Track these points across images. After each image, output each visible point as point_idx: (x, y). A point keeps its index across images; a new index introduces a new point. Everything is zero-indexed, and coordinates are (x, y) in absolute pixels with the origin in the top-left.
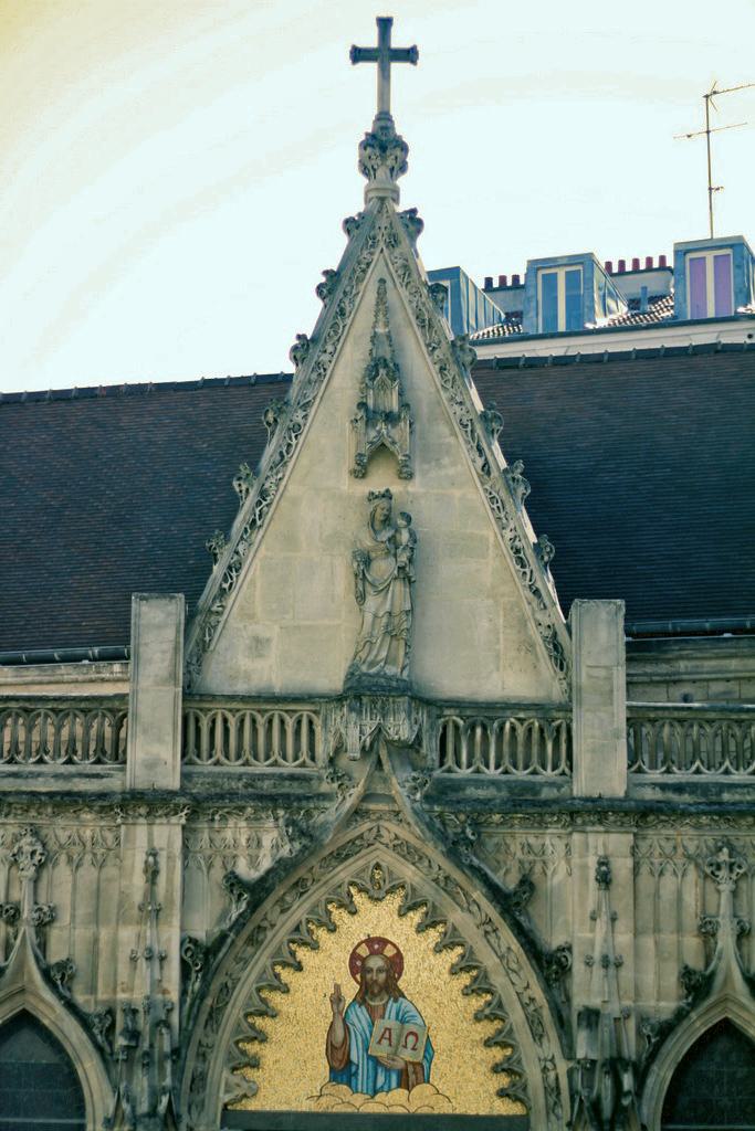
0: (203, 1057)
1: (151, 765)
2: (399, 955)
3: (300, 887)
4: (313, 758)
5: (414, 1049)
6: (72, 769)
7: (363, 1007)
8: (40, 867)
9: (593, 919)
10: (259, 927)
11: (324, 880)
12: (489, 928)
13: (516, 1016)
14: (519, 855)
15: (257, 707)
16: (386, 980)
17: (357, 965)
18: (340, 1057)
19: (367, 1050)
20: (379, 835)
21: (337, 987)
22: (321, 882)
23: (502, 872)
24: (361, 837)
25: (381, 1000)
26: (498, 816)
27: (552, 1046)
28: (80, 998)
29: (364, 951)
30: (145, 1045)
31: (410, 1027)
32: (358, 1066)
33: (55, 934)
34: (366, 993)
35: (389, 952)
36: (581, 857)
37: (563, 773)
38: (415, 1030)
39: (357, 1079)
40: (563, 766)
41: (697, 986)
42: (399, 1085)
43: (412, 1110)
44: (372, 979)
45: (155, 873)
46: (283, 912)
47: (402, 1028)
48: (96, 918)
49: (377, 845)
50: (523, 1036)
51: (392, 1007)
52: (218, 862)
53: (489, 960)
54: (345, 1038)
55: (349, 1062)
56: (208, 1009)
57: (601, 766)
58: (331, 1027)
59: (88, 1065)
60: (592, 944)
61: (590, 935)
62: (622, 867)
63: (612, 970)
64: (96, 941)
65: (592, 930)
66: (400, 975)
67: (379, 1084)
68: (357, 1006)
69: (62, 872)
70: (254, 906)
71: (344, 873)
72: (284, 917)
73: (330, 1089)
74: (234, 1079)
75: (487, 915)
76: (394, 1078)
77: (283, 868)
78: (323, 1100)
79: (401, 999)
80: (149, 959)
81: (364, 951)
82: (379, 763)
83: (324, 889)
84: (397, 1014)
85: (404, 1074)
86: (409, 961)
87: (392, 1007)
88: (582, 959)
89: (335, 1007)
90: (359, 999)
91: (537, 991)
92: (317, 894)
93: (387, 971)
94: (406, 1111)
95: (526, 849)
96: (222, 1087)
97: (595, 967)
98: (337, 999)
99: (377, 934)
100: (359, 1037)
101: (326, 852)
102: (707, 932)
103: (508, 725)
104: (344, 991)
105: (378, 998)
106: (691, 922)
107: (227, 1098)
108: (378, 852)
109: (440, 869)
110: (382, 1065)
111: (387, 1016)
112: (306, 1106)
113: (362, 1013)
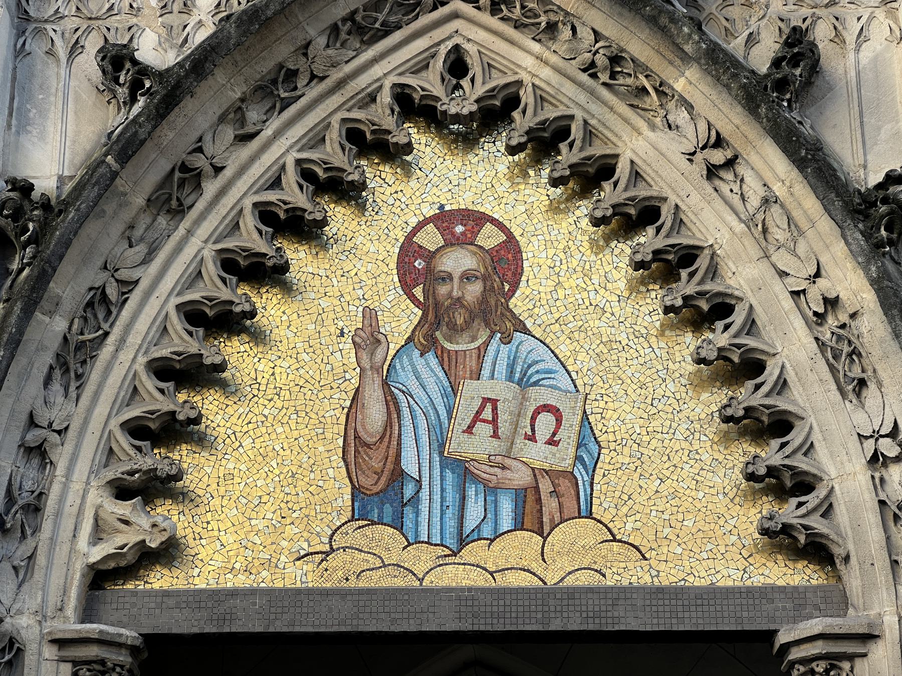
2: (511, 246)
3: (278, 89)
5: (552, 442)
10: (184, 168)
13: (792, 346)
16: (483, 300)
17: (415, 268)
19: (442, 446)
21: (370, 315)
25: (474, 339)
29: (430, 238)
31: (539, 396)
32: (419, 482)
34: (437, 323)
35: (489, 238)
39: (417, 513)
42: (519, 525)
43: (552, 579)
53: (711, 222)
54: (389, 424)
55: (398, 475)
67: (470, 524)
73: (355, 536)
74: (124, 508)
76: (506, 507)
81: (430, 238)
86: (534, 255)
87: (499, 354)
89: (364, 356)
93: (485, 278)
98: (369, 338)
99: (465, 200)
107: (97, 554)
110: (476, 479)
111: (486, 372)
113: (429, 368)
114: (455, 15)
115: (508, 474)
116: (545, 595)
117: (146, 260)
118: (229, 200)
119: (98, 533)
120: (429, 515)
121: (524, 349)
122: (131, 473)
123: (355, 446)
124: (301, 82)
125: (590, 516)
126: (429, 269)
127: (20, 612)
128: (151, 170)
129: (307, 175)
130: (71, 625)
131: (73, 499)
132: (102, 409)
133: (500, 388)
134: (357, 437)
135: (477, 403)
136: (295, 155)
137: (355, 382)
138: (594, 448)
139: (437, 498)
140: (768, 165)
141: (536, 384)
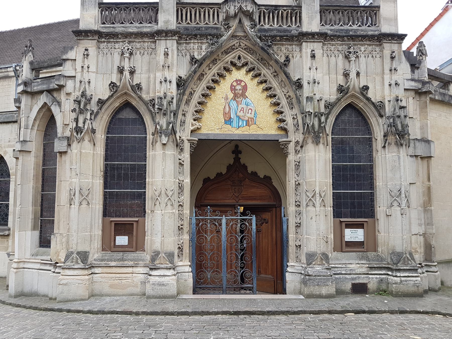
0: (184, 115)
1: (167, 22)
3: (214, 62)
4: (218, 22)
5: (251, 114)
6: (141, 25)
8: (131, 54)
9: (310, 69)
12: (275, 74)
13: (284, 102)
15: (208, 26)
16: (242, 93)
17: (233, 88)
26: (278, 38)
27: (296, 111)
28: (144, 96)
29: (235, 84)
30: (165, 107)
31: (249, 107)
33: (136, 76)
35: (243, 84)
36: (306, 49)
37: (298, 27)
40: (298, 24)
41: (341, 89)
45: (168, 54)
46: (209, 69)
48: (149, 71)
51: (244, 101)
52: (188, 54)
53: (274, 84)
55: (230, 118)
57: (311, 22)
59: (147, 117)
62: (319, 53)
64: (149, 77)
66: (246, 91)
67: (240, 125)
69: (138, 57)
71: (229, 58)
76: (245, 122)
80: (166, 81)
81: (235, 84)
82: (240, 21)
83: (222, 63)
87: (244, 101)
88: (307, 81)
91: (291, 94)
92: (220, 65)
95: (287, 50)
96: (190, 125)
98: (227, 98)
99: (240, 78)
102: (346, 75)
103: (280, 12)
106: (341, 72)
107: (192, 128)
112: (217, 132)
114: (239, 50)
118: (208, 78)
119: (192, 125)
120: (235, 124)
123: (225, 114)
128: (198, 74)
130: (189, 138)
132: (191, 109)
133: (244, 106)
140: (282, 76)
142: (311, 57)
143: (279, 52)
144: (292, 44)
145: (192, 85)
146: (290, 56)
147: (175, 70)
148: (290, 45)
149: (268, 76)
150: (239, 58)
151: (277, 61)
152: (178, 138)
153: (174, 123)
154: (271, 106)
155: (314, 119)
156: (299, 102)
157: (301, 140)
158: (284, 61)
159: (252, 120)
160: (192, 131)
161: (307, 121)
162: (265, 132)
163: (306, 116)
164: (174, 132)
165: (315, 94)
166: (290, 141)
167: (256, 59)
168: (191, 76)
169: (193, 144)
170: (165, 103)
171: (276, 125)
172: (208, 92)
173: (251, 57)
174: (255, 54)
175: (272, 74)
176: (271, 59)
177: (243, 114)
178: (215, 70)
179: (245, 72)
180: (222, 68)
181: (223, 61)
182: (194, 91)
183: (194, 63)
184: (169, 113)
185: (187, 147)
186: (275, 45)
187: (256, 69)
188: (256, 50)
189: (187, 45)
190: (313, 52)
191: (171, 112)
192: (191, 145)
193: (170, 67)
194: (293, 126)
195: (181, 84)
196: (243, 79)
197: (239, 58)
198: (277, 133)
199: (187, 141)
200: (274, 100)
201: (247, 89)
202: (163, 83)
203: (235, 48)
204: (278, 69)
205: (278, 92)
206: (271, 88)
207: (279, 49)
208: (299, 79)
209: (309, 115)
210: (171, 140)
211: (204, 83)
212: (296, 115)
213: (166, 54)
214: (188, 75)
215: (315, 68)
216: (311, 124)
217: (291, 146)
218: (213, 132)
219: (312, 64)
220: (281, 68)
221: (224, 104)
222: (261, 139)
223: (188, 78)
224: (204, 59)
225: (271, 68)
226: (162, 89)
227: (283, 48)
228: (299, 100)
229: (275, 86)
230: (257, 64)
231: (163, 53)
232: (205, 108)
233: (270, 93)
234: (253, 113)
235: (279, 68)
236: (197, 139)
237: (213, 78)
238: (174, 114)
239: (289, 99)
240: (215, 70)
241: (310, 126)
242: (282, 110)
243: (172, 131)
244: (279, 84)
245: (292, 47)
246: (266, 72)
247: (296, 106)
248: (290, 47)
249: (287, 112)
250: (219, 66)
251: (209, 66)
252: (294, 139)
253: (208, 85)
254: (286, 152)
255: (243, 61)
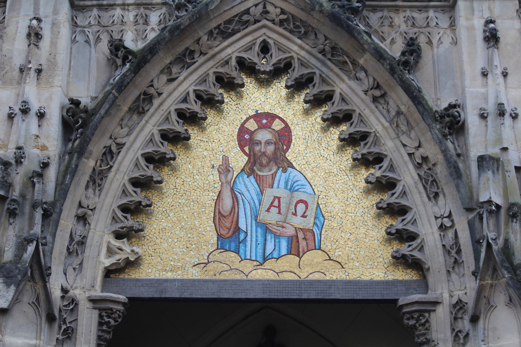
0: (82, 219)
3: (185, 59)
5: (304, 216)
7: (252, 177)
9: (485, 74)
10: (145, 94)
11: (211, 53)
12: (377, 93)
13: (408, 177)
14: (403, 27)
18: (228, 225)
19: (256, 217)
20: (266, 12)
21: (225, 159)
22: (208, 56)
23: (388, 41)
24: (247, 12)
25: (270, 170)
27: (449, 203)
29: (252, 125)
30: (15, 194)
32: (246, 233)
35: (277, 125)
38: (304, 198)
39: (246, 247)
42: (289, 253)
43: (303, 276)
44: (260, 151)
45: (38, 36)
46: (171, 80)
47: (292, 197)
49: (264, 22)
50: (417, 200)
53: (376, 122)
54: (233, 207)
55: (237, 229)
56: (89, 171)
58: (219, 196)
60: (486, 99)
61: (483, 90)
63: (507, 120)
65: (486, 85)
67: (268, 252)
68: (246, 176)
70: (137, 69)
71: (233, 49)
72: (167, 90)
73: (218, 256)
75: (374, 79)
77: (172, 35)
78: (210, 266)
79: (290, 169)
81: (252, 125)
83: (211, 63)
84: (286, 183)
85: (294, 238)
86: (297, 132)
88: (477, 112)
90: (247, 169)
91: (431, 150)
93: (275, 144)
94: (298, 278)
95: (410, 23)
96: (101, 249)
97: (489, 119)
98: (225, 169)
99: (267, 109)
100: (246, 202)
101: (213, 24)
104: (233, 164)
105: (267, 169)
107: (108, 262)
108: (264, 30)
109: (326, 38)
110: (271, 232)
111: (275, 185)
112: (195, 274)
114: (264, 26)
115: (284, 230)
116: (300, 283)
117: (128, 135)
119: (110, 252)
121: (292, 175)
122: (122, 228)
123: (219, 216)
124: (196, 55)
125: (320, 249)
126: (251, 139)
127: (76, 288)
128: (132, 95)
129: (199, 96)
130: (97, 293)
131: (96, 238)
132: (109, 200)
134: (220, 213)
135: (272, 198)
136: (193, 88)
137: (219, 189)
138: (322, 219)
139: (254, 240)
140: (399, 99)
141: (297, 190)
142: (487, 39)
143: (386, 29)
144: (426, 7)
145: (112, 126)
146: (422, 40)
147: (59, 79)
148: (420, 9)
149: (355, 99)
150: (265, 49)
151: (380, 55)
152: (56, 293)
153: (42, 244)
154: (367, 192)
155: (507, 224)
156: (456, 173)
157: (470, 299)
158: (403, 54)
159: (309, 235)
160: (109, 273)
161: (486, 231)
162: (353, 275)
163: (481, 219)
164: (40, 271)
165: (505, 149)
166: (436, 303)
167: (315, 51)
168: (110, 99)
169: (110, 312)
170: (18, 177)
171: (386, 252)
172: (166, 148)
173: (300, 47)
174: (313, 36)
175: (366, 92)
176: (362, 48)
177: (279, 217)
178: (188, 83)
179: (284, 92)
180: (212, 78)
181: (214, 56)
182: (120, 146)
183: (119, 62)
184: (27, 209)
185: (87, 323)
186: (374, 9)
187: (317, 80)
188: (314, 23)
189: (103, 14)
190: (492, 25)
191: (34, 206)
192: (101, 316)
193: (43, 74)
194: (440, 251)
195: (77, 121)
196: (277, 111)
197: (265, 49)
198: (390, 278)
199: (89, 305)
200: (376, 172)
201: (290, 141)
202: (18, 119)
203: (252, 19)
204: (381, 74)
205: (389, 146)
206: (364, 136)
207: (387, 23)
208: (452, 106)
209: (490, 212)
210: (28, 297)
211: (153, 120)
212: (450, 216)
213: (34, 36)
214: (101, 96)
215: (499, 71)
216: (501, 242)
217: (440, 321)
218: (178, 275)
219: (490, 61)
220: (392, 71)
221: (218, 185)
222: (337, 296)
223: (100, 105)
224: (152, 50)
225: (362, 75)
226: (13, 138)
227: (399, 19)
228: (457, 169)
229: (379, 128)
230: (319, 65)
231: (25, 31)
232: (155, 199)
233: (362, 150)
234: (311, 213)
235: (387, 75)
236: (122, 298)
237: (183, 106)
238: (46, 215)
239: (425, 167)
240: (188, 83)
241: (495, 248)
242: (404, 202)
243: (35, 267)
244: (391, 122)
245: (424, 15)
246: (348, 89)
247: (448, 187)
248: (419, 16)
249: (421, 208)
250: (200, 72)
251: (170, 73)
252: (446, 295)
253: (165, 127)
254: (422, 339)
255: (276, 57)
